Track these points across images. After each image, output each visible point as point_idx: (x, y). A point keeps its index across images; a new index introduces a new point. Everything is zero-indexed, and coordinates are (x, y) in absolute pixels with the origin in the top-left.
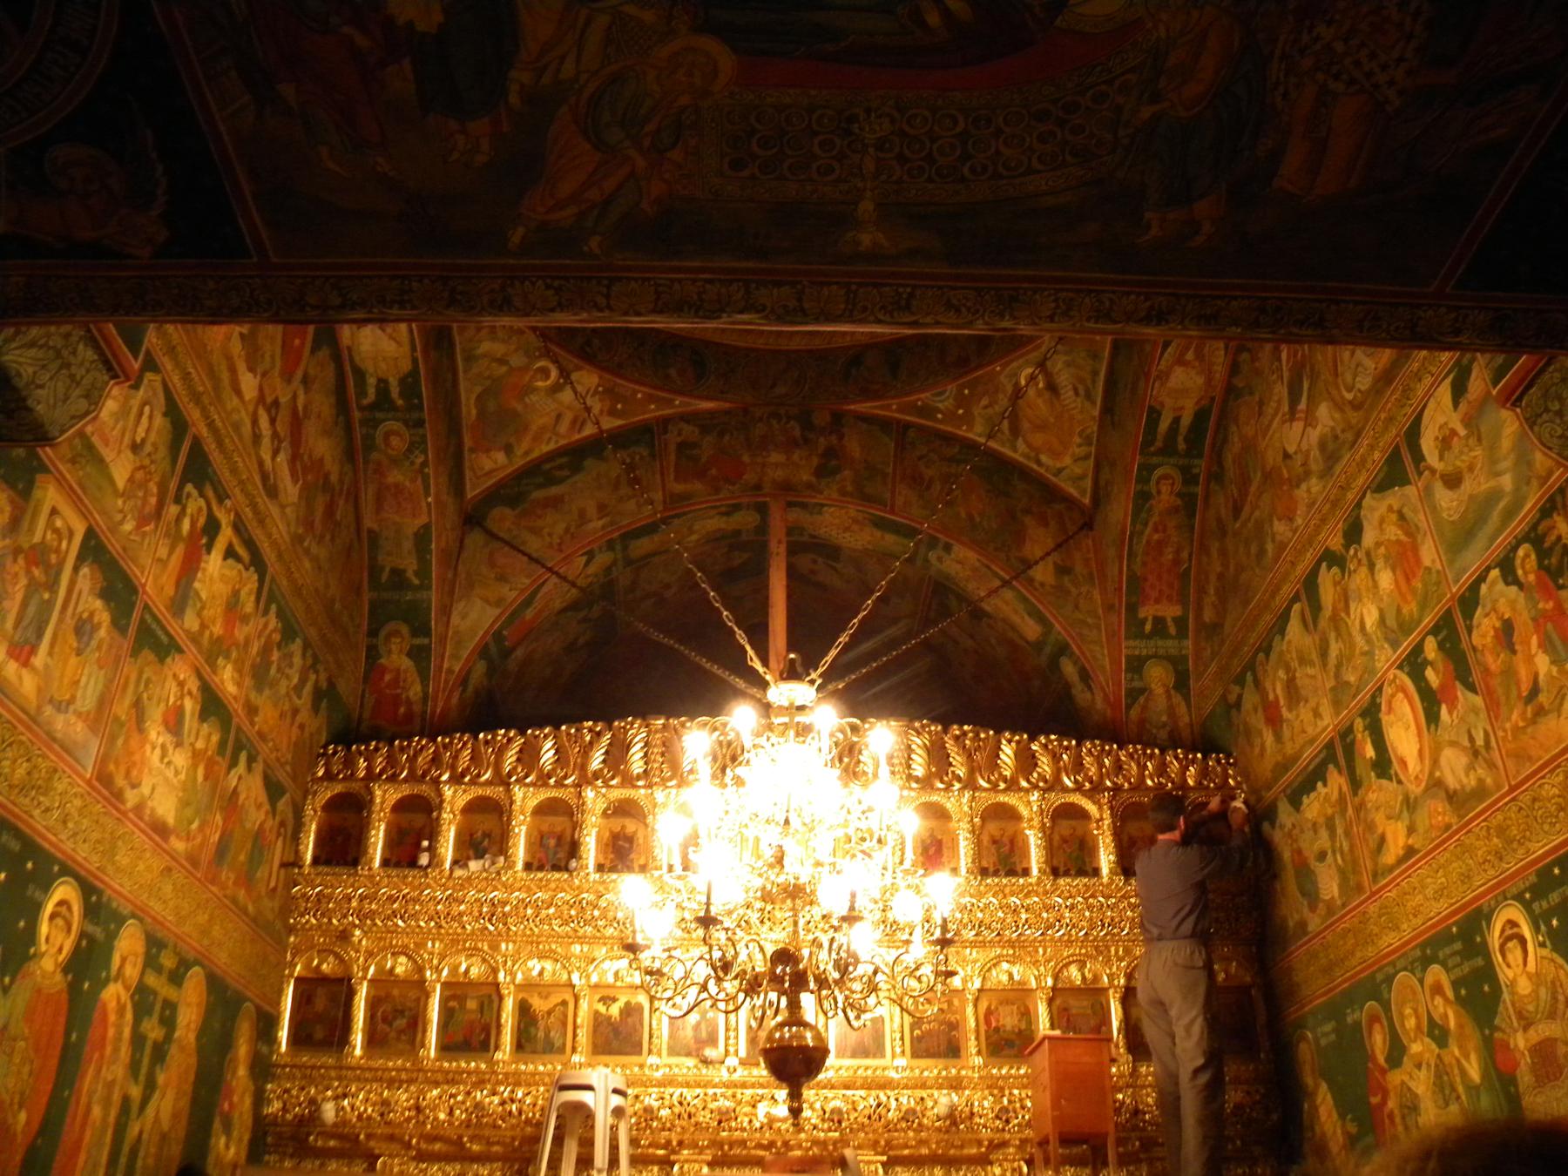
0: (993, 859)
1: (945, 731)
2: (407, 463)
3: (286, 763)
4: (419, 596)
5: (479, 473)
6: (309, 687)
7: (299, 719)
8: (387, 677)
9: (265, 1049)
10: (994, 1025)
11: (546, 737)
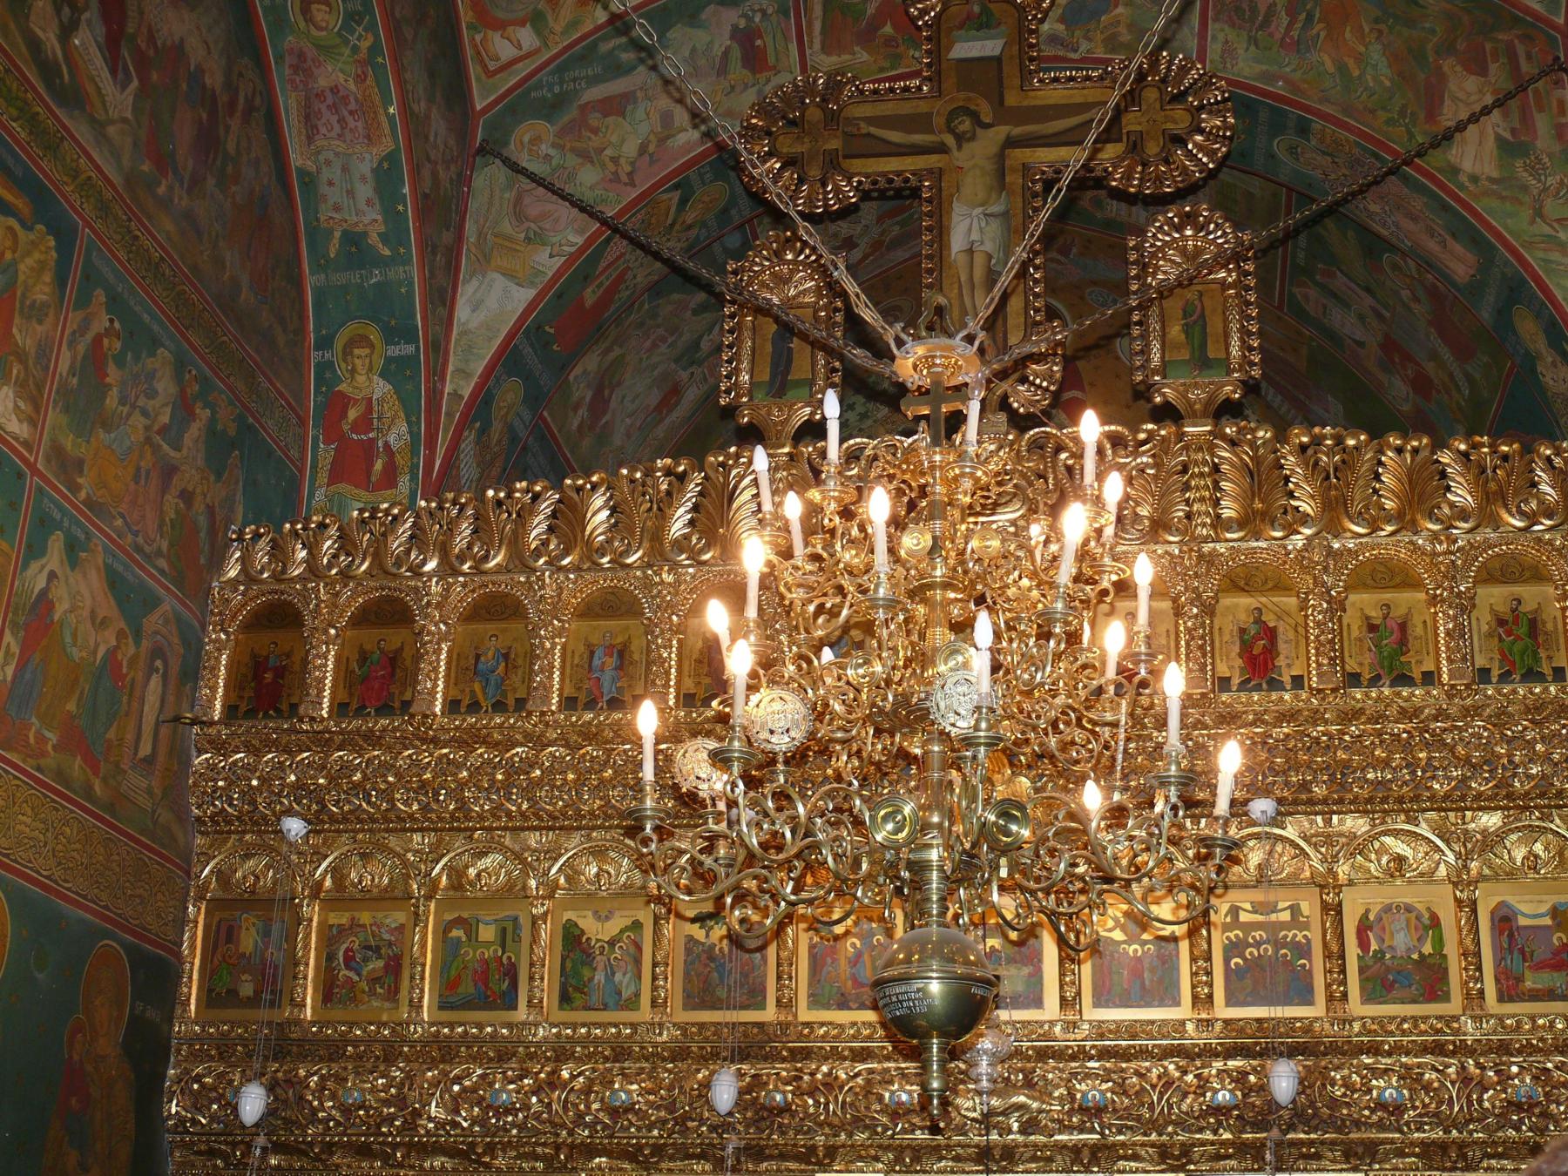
0: (1368, 659)
1: (1281, 436)
2: (347, 52)
3: (159, 553)
4: (391, 274)
5: (492, 66)
6: (194, 431)
7: (177, 483)
8: (352, 414)
9: (152, 1014)
10: (1374, 946)
11: (594, 487)
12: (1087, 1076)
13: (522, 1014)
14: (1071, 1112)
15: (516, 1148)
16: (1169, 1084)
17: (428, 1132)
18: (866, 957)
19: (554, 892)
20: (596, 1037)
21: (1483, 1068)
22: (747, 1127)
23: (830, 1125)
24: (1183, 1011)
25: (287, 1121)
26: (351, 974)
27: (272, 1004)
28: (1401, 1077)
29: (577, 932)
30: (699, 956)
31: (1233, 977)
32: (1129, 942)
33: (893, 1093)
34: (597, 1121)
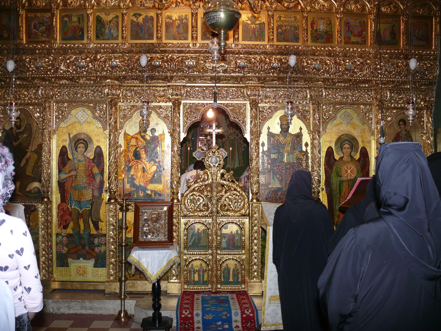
12: (241, 58)
13: (85, 41)
14: (236, 68)
15: (86, 77)
16: (261, 61)
17: (61, 73)
18: (181, 26)
19: (93, 7)
20: (107, 47)
21: (340, 60)
22: (149, 71)
23: (172, 70)
24: (266, 43)
25: (21, 71)
26: (36, 31)
27: (14, 39)
28: (320, 62)
29: (100, 19)
30: (135, 25)
31: (279, 34)
32: (252, 24)
33: (188, 62)
34: (108, 70)
